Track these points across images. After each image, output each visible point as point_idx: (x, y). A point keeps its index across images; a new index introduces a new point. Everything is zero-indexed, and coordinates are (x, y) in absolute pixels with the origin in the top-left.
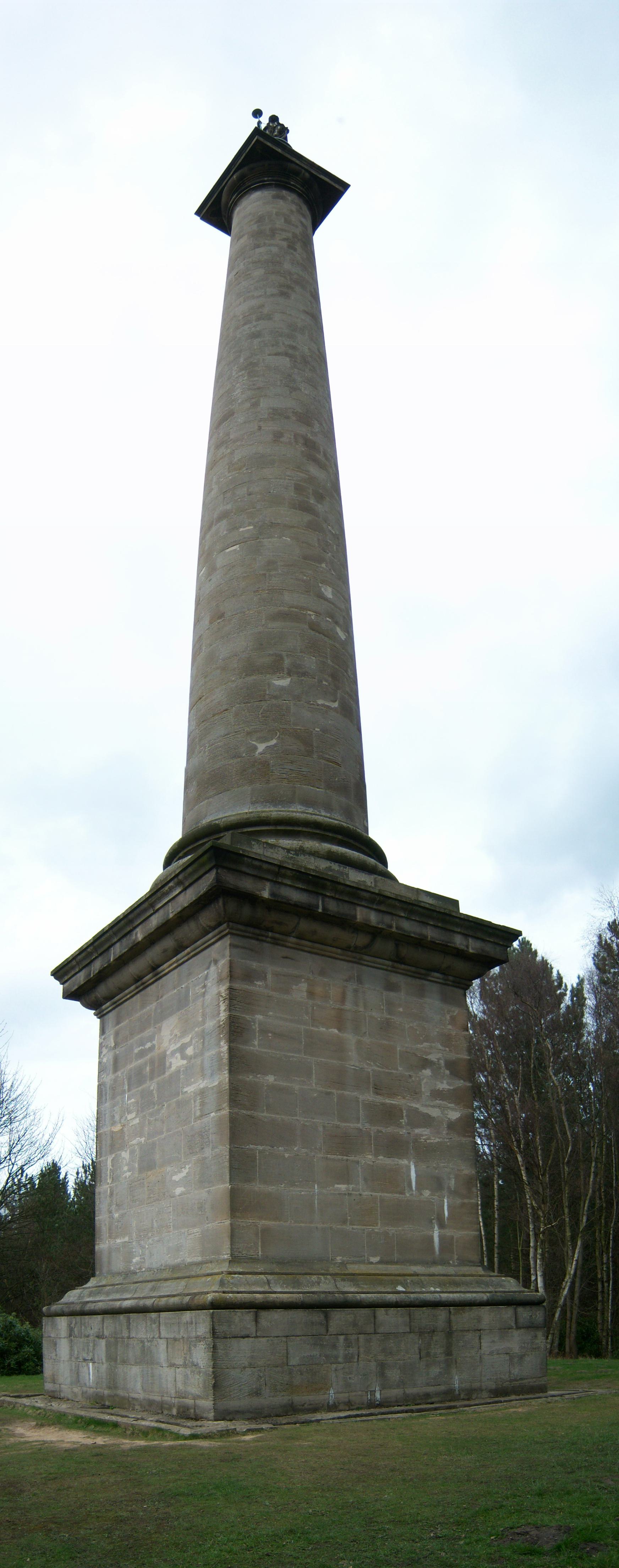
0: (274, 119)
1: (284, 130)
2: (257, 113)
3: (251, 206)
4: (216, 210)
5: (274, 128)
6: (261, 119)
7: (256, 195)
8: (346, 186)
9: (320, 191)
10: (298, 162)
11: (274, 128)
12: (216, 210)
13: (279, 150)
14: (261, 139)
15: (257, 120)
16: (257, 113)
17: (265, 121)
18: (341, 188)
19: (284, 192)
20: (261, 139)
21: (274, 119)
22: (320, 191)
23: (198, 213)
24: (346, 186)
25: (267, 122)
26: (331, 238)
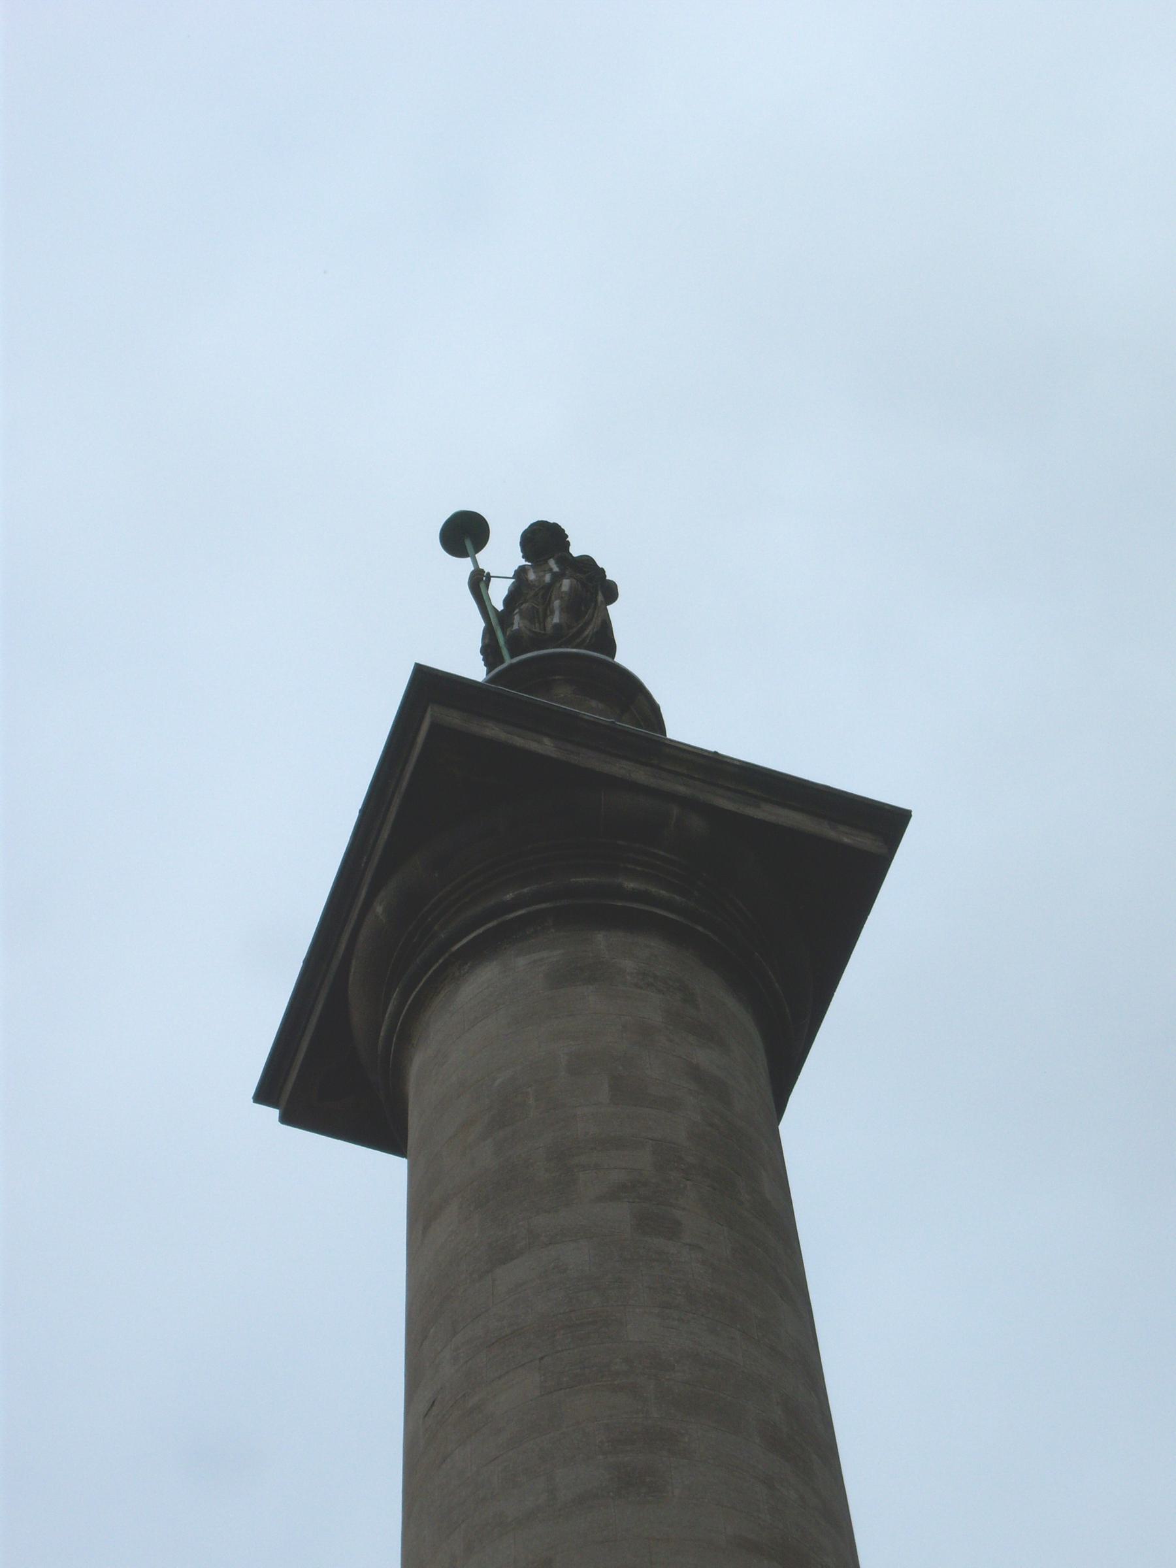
0: (544, 540)
1: (593, 587)
2: (464, 533)
3: (476, 1028)
4: (333, 1066)
5: (546, 592)
6: (487, 559)
7: (480, 983)
8: (888, 823)
9: (786, 879)
10: (641, 775)
11: (546, 592)
12: (333, 1066)
13: (546, 746)
14: (454, 719)
15: (465, 566)
16: (464, 533)
17: (503, 557)
18: (865, 841)
19: (602, 942)
20: (454, 719)
21: (544, 540)
22: (786, 879)
23: (265, 1095)
24: (888, 823)
25: (517, 560)
26: (864, 1132)
